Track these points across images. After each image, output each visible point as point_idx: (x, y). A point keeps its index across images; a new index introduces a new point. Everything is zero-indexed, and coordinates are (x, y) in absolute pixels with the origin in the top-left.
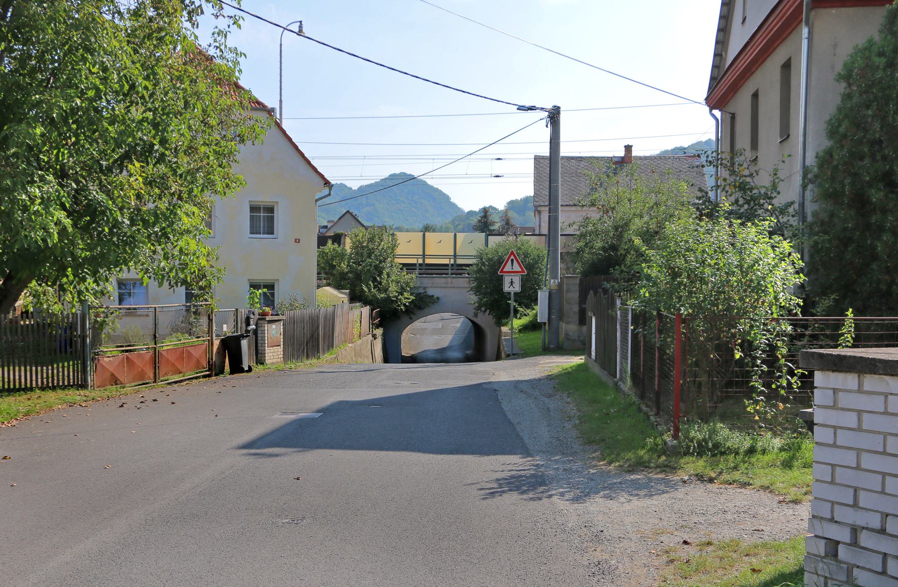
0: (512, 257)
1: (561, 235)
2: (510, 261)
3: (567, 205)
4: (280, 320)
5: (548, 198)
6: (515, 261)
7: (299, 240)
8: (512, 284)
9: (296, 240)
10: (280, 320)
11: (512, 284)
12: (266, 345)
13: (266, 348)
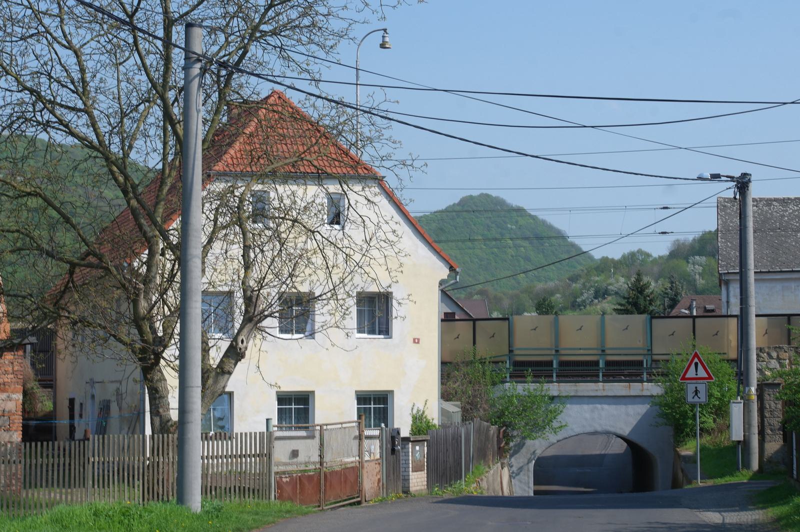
0: (696, 360)
1: (757, 316)
2: (693, 365)
3: (769, 272)
4: (424, 441)
5: (738, 261)
6: (699, 365)
7: (418, 340)
8: (696, 394)
9: (414, 340)
10: (424, 441)
11: (696, 394)
12: (411, 469)
13: (411, 473)
